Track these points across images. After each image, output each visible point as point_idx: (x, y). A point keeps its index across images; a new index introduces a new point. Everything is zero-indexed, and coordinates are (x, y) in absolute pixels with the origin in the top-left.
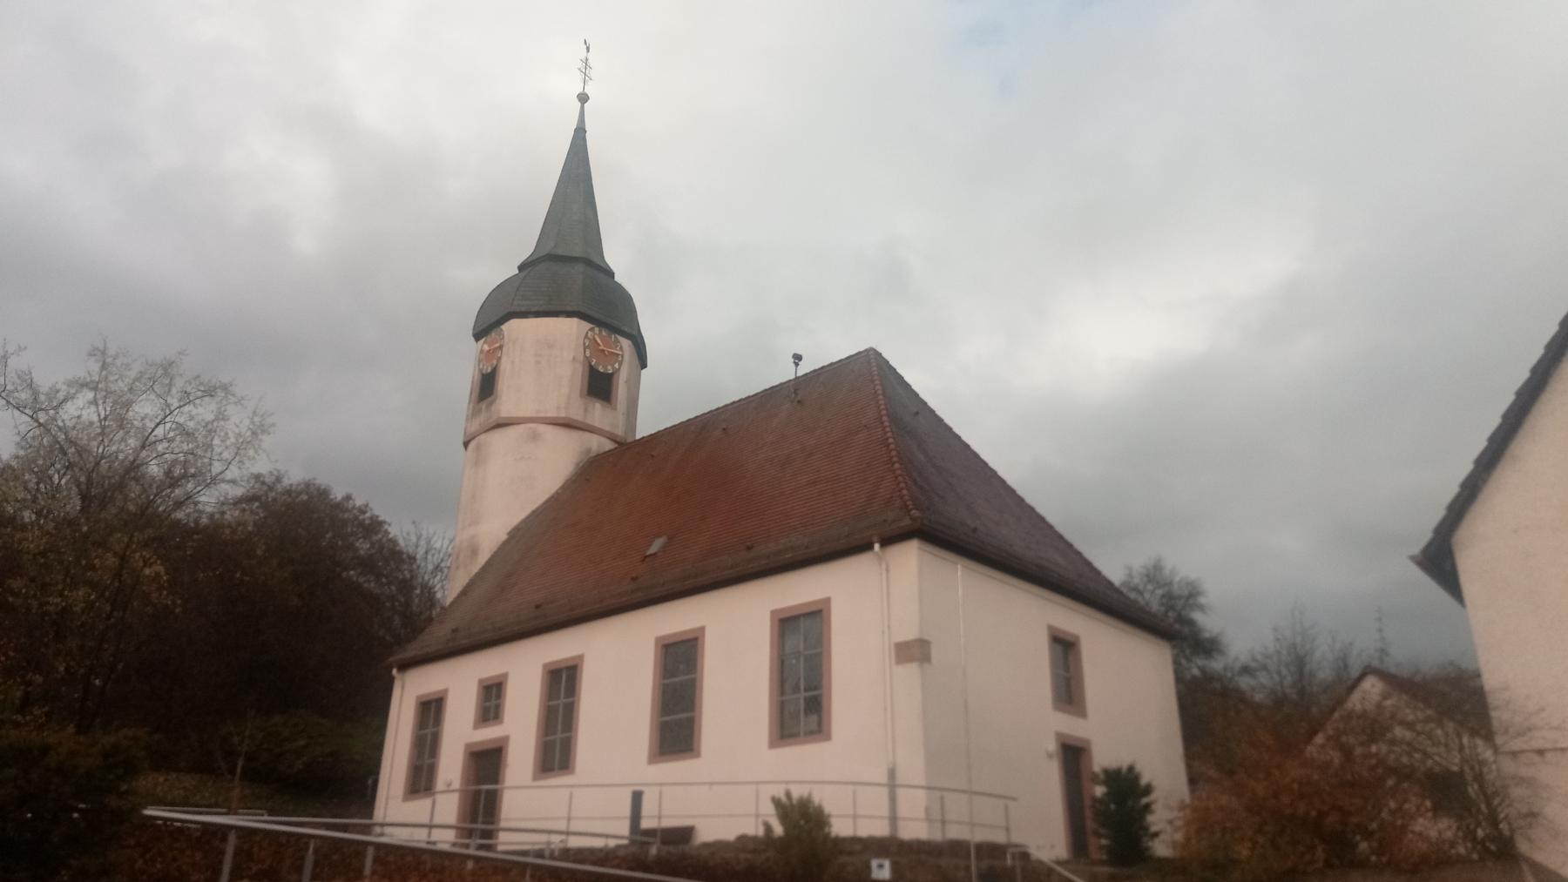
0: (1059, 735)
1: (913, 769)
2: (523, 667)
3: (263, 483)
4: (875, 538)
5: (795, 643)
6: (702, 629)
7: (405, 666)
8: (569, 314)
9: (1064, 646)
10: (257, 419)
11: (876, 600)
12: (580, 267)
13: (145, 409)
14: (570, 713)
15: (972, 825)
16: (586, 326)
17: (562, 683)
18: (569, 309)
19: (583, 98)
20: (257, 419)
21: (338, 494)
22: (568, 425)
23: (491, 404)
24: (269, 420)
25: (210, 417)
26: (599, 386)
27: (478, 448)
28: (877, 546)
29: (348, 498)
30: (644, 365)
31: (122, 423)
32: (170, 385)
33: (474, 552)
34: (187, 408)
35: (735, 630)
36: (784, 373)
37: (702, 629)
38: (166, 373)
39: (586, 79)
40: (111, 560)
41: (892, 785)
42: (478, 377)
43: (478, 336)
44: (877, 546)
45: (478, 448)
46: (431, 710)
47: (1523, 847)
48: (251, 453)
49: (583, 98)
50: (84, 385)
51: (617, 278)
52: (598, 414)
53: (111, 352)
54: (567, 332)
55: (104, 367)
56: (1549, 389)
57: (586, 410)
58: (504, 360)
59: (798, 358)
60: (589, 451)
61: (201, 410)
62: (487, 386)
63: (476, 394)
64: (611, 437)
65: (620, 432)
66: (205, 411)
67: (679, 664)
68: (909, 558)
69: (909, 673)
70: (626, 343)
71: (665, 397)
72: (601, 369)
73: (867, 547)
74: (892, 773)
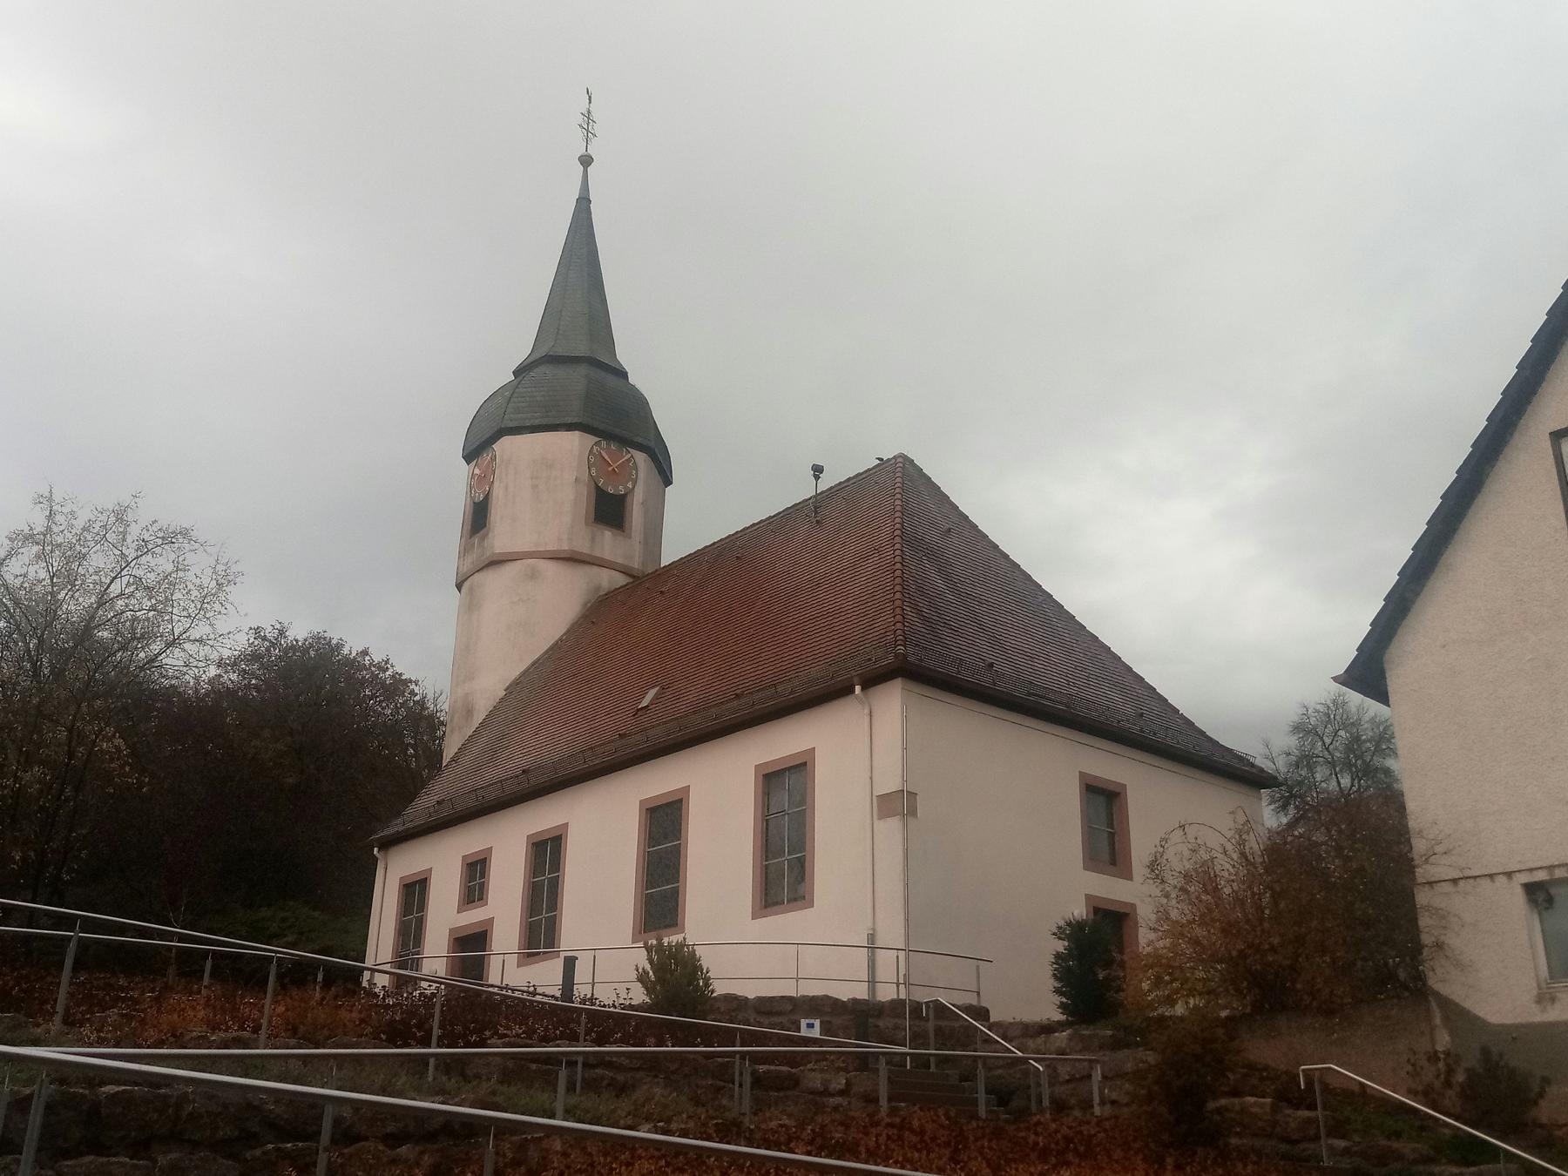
0: (1088, 897)
1: (892, 932)
2: (507, 841)
3: (264, 638)
4: (856, 680)
5: (782, 800)
6: (687, 789)
7: (388, 844)
8: (570, 427)
9: (1104, 801)
10: (220, 568)
11: (856, 750)
12: (582, 370)
13: (99, 560)
14: (555, 887)
15: (907, 984)
16: (593, 439)
17: (547, 854)
18: (569, 420)
19: (586, 161)
20: (220, 568)
21: (352, 647)
22: (572, 559)
23: (483, 539)
24: (234, 569)
25: (170, 568)
26: (608, 510)
27: (471, 589)
28: (858, 689)
29: (365, 653)
30: (668, 481)
31: (71, 581)
32: (124, 534)
33: (469, 712)
34: (143, 560)
35: (718, 789)
36: (803, 489)
37: (687, 789)
38: (119, 519)
39: (589, 135)
40: (63, 735)
41: (872, 948)
42: (470, 509)
43: (469, 457)
44: (858, 689)
45: (471, 589)
46: (415, 892)
47: (1433, 982)
48: (217, 606)
49: (586, 161)
50: (29, 538)
51: (633, 379)
52: (608, 544)
53: (57, 498)
54: (570, 447)
55: (51, 516)
56: (1485, 490)
57: (593, 540)
58: (496, 484)
59: (818, 470)
60: (598, 588)
61: (160, 560)
62: (479, 517)
63: (468, 527)
64: (625, 571)
65: (636, 564)
66: (163, 562)
67: (664, 824)
68: (892, 705)
69: (891, 828)
70: (640, 458)
71: (697, 515)
72: (611, 490)
73: (846, 691)
74: (872, 938)
